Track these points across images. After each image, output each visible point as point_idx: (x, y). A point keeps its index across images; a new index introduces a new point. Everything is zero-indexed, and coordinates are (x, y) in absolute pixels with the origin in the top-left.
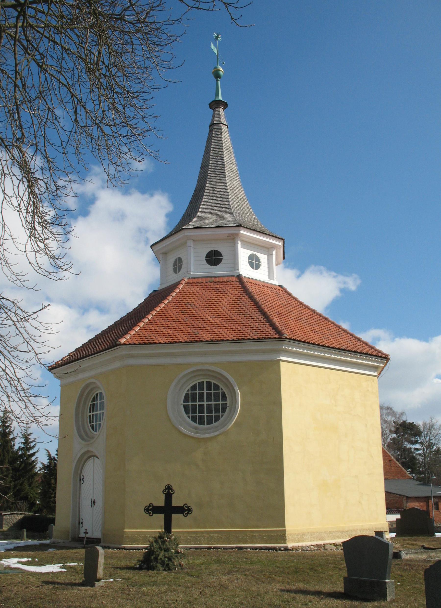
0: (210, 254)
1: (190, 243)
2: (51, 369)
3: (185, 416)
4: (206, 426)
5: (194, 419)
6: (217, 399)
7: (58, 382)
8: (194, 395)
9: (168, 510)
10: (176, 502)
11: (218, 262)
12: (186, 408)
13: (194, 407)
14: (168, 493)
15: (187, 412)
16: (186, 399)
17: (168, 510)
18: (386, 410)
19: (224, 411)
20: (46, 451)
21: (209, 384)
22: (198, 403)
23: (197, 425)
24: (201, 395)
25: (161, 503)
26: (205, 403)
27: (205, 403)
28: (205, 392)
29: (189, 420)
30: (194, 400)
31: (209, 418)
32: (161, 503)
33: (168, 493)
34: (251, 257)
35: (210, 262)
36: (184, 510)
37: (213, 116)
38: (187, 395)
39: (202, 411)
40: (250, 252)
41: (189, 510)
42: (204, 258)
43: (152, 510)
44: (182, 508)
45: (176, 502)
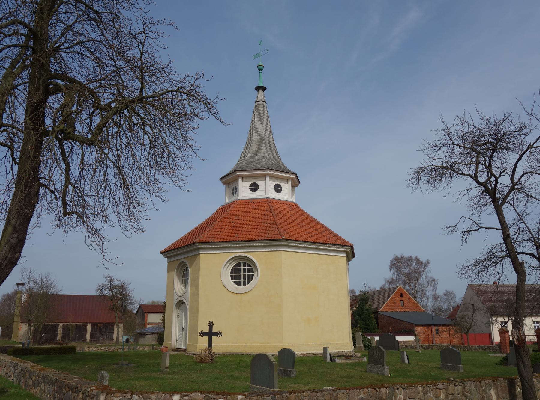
0: (252, 185)
1: (240, 180)
2: (162, 253)
3: (231, 281)
4: (242, 287)
5: (236, 283)
6: (248, 272)
7: (166, 260)
8: (236, 270)
9: (211, 334)
10: (215, 330)
11: (256, 189)
12: (232, 276)
13: (236, 276)
15: (232, 279)
16: (232, 272)
19: (252, 279)
20: (221, 116)
21: (240, 285)
22: (238, 274)
23: (237, 286)
24: (240, 270)
28: (242, 268)
29: (233, 283)
34: (276, 186)
35: (252, 190)
36: (218, 334)
37: (257, 96)
38: (232, 269)
39: (240, 278)
40: (276, 183)
41: (221, 334)
42: (249, 187)
44: (217, 333)
45: (215, 330)
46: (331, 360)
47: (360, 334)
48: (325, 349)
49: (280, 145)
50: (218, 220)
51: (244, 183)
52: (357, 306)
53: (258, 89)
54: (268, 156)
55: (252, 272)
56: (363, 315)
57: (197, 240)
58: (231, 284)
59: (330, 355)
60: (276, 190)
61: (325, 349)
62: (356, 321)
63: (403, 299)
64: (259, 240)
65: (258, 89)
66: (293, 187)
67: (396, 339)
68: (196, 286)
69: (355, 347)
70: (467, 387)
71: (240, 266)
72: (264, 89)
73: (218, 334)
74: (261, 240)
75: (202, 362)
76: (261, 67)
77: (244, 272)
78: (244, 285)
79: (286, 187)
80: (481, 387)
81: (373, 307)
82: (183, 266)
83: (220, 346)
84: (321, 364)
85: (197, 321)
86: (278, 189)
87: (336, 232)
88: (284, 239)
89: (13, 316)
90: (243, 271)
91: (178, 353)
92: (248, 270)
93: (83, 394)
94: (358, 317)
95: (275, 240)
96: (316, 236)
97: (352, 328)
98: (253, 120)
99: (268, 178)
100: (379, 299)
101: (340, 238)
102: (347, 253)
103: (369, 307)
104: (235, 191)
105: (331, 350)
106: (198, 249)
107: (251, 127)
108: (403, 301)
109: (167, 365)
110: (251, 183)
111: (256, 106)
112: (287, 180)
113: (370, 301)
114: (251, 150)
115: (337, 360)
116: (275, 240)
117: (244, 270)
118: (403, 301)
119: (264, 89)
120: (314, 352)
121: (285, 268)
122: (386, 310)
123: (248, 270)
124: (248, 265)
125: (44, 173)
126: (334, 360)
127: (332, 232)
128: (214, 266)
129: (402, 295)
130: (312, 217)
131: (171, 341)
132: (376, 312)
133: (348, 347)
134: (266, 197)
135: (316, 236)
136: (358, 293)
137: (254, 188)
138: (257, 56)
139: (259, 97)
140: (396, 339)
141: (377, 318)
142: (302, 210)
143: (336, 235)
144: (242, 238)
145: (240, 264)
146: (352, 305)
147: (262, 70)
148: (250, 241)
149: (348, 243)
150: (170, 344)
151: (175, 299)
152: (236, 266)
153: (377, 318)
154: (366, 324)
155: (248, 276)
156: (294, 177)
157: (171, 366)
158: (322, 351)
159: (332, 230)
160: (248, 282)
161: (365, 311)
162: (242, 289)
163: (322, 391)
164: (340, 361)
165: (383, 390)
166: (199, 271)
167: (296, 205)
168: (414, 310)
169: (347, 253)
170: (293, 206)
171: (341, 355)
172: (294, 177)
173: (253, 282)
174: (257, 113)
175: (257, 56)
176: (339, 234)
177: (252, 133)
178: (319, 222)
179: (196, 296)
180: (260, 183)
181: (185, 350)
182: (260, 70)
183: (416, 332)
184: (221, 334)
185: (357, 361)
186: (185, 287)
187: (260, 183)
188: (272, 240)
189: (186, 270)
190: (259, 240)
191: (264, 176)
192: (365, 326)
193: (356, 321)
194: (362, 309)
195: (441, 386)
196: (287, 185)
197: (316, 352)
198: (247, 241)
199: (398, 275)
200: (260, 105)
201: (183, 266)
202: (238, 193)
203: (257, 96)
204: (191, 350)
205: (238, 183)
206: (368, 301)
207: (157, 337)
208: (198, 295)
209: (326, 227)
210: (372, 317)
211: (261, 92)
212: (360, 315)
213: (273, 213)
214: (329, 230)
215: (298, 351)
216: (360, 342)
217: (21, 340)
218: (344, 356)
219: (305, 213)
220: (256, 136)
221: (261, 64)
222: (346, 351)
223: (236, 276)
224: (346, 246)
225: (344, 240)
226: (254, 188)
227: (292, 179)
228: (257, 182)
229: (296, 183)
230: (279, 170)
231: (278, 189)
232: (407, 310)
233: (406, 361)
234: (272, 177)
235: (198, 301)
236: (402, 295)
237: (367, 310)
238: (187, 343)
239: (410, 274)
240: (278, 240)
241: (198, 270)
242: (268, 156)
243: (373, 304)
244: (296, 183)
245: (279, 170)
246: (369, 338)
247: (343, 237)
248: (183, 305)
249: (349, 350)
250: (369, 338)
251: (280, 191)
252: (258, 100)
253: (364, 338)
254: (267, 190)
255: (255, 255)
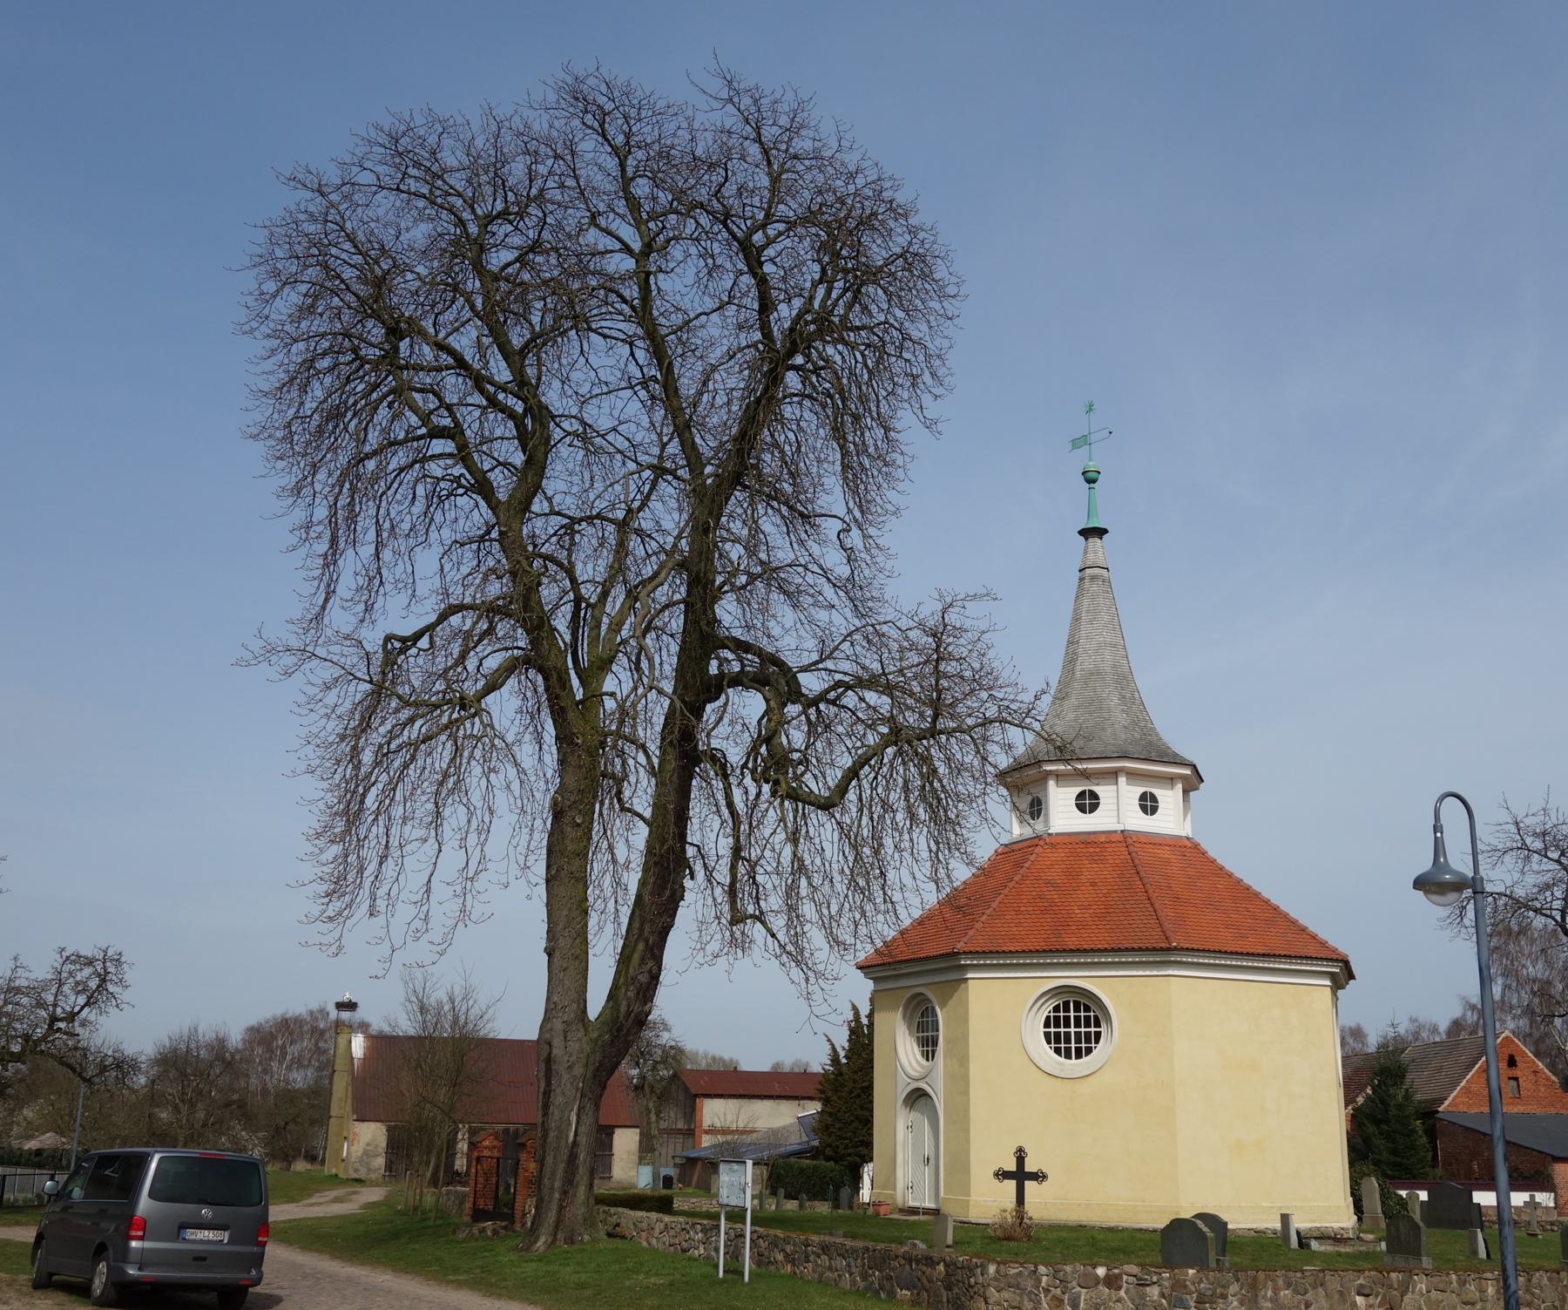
0: (1081, 795)
3: (1047, 1046)
4: (1074, 1061)
5: (1058, 1051)
6: (1088, 1025)
7: (870, 985)
8: (1057, 1019)
9: (1020, 1175)
12: (1047, 1035)
13: (1057, 1035)
14: (1020, 1156)
15: (1049, 1042)
16: (1047, 1025)
17: (1020, 1175)
18: (1352, 1035)
19: (1097, 1042)
21: (1068, 1056)
23: (1062, 1059)
25: (1012, 1167)
26: (1072, 1030)
27: (1072, 1030)
29: (1052, 1053)
30: (1057, 1025)
31: (1079, 1050)
32: (1012, 1167)
33: (1020, 1156)
34: (1143, 797)
35: (1081, 808)
36: (1038, 1177)
37: (1086, 552)
38: (1048, 1018)
39: (1068, 1041)
40: (1142, 790)
41: (996, 1175)
43: (1003, 1175)
46: (1301, 1244)
47: (1372, 1185)
48: (1285, 1219)
49: (1147, 683)
50: (1006, 891)
51: (1061, 790)
52: (1369, 1091)
53: (1087, 533)
54: (1121, 718)
55: (1098, 1024)
56: (1387, 1122)
57: (960, 946)
58: (1045, 1053)
59: (1298, 1233)
60: (1144, 809)
61: (1285, 1219)
62: (1366, 1140)
63: (1517, 1072)
64: (1113, 950)
65: (1087, 533)
66: (1186, 792)
67: (1475, 1200)
68: (961, 1058)
69: (1360, 1219)
70: (1534, 1280)
71: (1067, 1009)
72: (1100, 532)
73: (1038, 1177)
74: (1120, 950)
75: (1008, 1239)
76: (1092, 475)
77: (1067, 1035)
78: (1079, 1055)
79: (1169, 798)
80: (1561, 1281)
81: (1418, 1097)
82: (919, 1004)
83: (1043, 1203)
84: (1281, 1251)
85: (968, 1141)
86: (1149, 805)
87: (1303, 921)
88: (1175, 949)
89: (319, 1096)
90: (1075, 1024)
91: (921, 1217)
92: (1087, 1019)
93: (947, 1266)
94: (1371, 1128)
95: (1154, 949)
96: (1252, 935)
97: (1351, 1164)
98: (1076, 619)
99: (1122, 780)
100: (1440, 1069)
101: (1314, 937)
102: (1332, 976)
103: (1407, 1096)
104: (1037, 808)
105: (1299, 1223)
106: (966, 968)
107: (1072, 635)
108: (1516, 1079)
109: (950, 1241)
110: (1079, 789)
111: (1082, 579)
112: (1171, 780)
113: (1409, 1077)
114: (1073, 701)
115: (1314, 1245)
116: (1154, 949)
117: (1077, 1019)
118: (1516, 1079)
119: (1100, 532)
120: (1254, 1226)
121: (1176, 1017)
122: (1462, 1108)
123: (1087, 1019)
124: (1087, 1009)
125: (694, 834)
126: (1308, 1246)
127: (1294, 922)
128: (1002, 1009)
129: (1512, 1062)
130: (1239, 881)
131: (894, 1189)
132: (1428, 1114)
133: (1341, 1217)
134: (1120, 827)
135: (1252, 935)
136: (1372, 1043)
137: (1087, 803)
138: (1080, 442)
139: (1091, 556)
140: (1475, 1200)
141: (1432, 1134)
142: (1213, 861)
143: (1304, 929)
144: (1072, 942)
145: (1066, 1004)
146: (1350, 1086)
147: (1094, 481)
148: (1092, 950)
149: (1334, 951)
150: (893, 1197)
151: (900, 1086)
152: (1056, 1009)
153: (1432, 1134)
154: (1394, 1152)
155: (1088, 1034)
156: (1187, 772)
157: (955, 1243)
158: (1278, 1226)
159: (1294, 914)
160: (1089, 1051)
161: (1393, 1112)
162: (1074, 1066)
163: (1302, 1271)
164: (1323, 1248)
165: (1393, 1275)
166: (966, 1021)
167: (1196, 846)
168: (1553, 1111)
169: (1332, 976)
170: (1188, 850)
171: (1323, 1237)
172: (1187, 772)
173: (1100, 1050)
174: (1086, 602)
175: (1080, 442)
176: (1312, 928)
177: (1074, 653)
178: (1257, 895)
179: (960, 1081)
180: (1104, 791)
181: (936, 1212)
182: (1091, 481)
183: (1558, 1180)
184: (1045, 1177)
185: (1363, 1248)
186: (929, 1055)
187: (1104, 791)
188: (1147, 949)
189: (929, 1012)
190: (1113, 950)
191: (1113, 775)
192: (1392, 1158)
193: (1366, 1140)
194: (1383, 1102)
195: (1489, 1275)
196: (1170, 793)
197: (1261, 1226)
198: (1085, 951)
199: (1506, 987)
200: (1093, 578)
201: (919, 1004)
202: (1047, 815)
203: (1086, 552)
204: (954, 1212)
205: (1046, 789)
206: (1403, 1077)
207: (765, 1176)
208: (965, 1079)
209: (1276, 909)
210: (1414, 1131)
211: (1095, 542)
212: (1377, 1122)
213: (1143, 874)
214: (1286, 916)
215: (1238, 1220)
216: (1374, 1203)
217: (356, 1170)
218: (1329, 1238)
219: (1222, 868)
220: (1085, 663)
221: (1092, 466)
222: (1336, 1225)
223: (1057, 1035)
224: (1331, 960)
225: (1323, 944)
226: (1087, 803)
227: (1183, 778)
228: (1096, 789)
229: (1193, 781)
230: (1157, 761)
231: (1149, 805)
232: (1528, 1109)
233: (1482, 1253)
234: (1133, 776)
235: (967, 1093)
236: (1512, 1062)
237: (1400, 1107)
238: (942, 1194)
239: (1549, 983)
240: (1162, 949)
241: (964, 1020)
242: (1121, 718)
243: (1421, 1085)
244: (1193, 781)
245: (1157, 761)
246: (1403, 1193)
247: (1323, 935)
248: (922, 1101)
249: (1343, 1225)
250: (1403, 1193)
251: (1154, 810)
252: (1089, 564)
253: (1385, 1196)
254: (1119, 809)
255: (1100, 983)
